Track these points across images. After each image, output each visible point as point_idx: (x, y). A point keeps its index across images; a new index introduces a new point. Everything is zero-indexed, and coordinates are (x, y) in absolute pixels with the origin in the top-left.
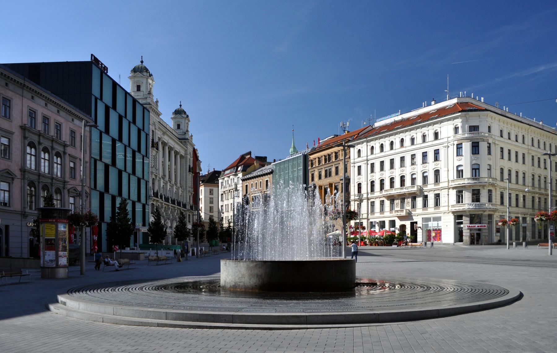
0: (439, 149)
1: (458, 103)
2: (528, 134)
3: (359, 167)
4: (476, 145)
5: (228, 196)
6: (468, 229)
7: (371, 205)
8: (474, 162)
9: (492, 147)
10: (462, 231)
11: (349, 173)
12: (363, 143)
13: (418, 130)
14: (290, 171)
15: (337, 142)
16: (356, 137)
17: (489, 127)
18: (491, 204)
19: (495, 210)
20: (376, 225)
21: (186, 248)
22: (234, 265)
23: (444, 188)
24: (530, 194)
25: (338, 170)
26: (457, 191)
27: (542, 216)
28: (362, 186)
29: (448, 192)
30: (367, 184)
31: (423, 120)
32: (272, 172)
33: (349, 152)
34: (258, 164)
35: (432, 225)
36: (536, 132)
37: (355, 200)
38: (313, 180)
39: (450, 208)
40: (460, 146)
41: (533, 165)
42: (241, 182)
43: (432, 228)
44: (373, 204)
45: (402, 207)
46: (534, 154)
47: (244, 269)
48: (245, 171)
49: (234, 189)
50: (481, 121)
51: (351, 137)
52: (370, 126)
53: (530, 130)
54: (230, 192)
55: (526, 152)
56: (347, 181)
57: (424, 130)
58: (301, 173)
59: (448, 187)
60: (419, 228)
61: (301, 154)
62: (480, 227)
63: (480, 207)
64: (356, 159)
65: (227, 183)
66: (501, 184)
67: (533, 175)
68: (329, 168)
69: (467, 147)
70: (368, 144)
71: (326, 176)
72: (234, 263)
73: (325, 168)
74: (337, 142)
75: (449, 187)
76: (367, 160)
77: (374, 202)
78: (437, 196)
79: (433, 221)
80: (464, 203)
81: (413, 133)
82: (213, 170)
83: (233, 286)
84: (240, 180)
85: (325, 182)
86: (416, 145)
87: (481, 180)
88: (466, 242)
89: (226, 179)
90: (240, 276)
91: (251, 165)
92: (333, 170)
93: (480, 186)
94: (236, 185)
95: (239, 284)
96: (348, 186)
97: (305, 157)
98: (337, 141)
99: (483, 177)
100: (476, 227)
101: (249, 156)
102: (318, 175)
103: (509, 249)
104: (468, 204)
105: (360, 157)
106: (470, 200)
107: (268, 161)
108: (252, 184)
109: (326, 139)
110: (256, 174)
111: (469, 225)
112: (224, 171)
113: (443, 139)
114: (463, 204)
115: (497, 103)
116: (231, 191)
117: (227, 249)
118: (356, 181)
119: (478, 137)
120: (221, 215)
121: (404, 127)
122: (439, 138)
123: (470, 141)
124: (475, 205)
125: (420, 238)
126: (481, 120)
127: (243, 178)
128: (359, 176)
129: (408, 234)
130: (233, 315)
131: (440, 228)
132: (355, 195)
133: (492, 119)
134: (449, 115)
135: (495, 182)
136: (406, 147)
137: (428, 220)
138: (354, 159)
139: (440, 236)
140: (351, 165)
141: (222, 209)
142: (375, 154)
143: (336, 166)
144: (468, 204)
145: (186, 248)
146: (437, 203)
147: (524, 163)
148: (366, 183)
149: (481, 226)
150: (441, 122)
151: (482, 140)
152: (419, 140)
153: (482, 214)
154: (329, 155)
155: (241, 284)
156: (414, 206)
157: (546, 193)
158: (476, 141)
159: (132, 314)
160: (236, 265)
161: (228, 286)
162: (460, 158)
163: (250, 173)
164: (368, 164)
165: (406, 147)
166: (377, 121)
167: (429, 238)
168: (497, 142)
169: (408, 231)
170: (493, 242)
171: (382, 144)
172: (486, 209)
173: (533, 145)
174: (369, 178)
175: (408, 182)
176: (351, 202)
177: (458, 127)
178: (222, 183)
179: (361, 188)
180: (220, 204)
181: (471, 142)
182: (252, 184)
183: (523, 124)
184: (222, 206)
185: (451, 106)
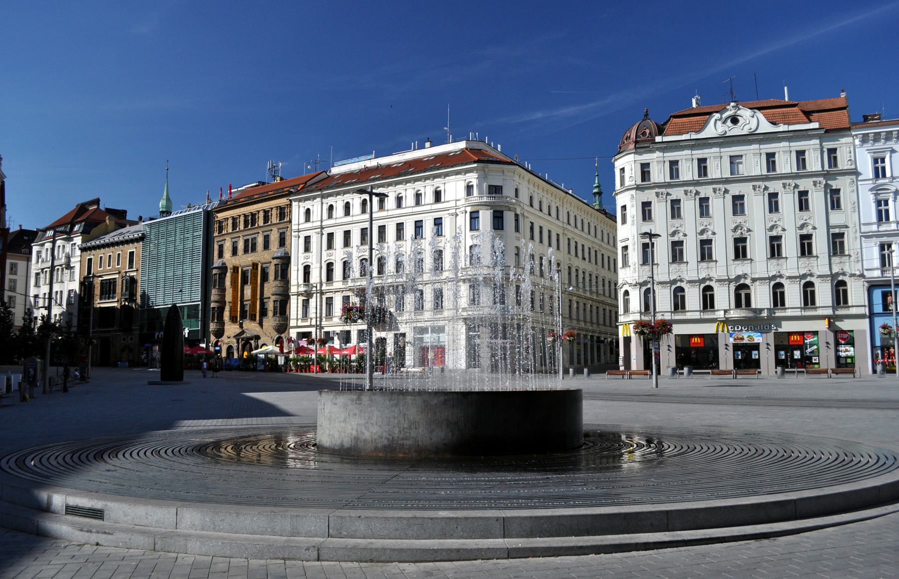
1: (466, 149)
2: (563, 206)
3: (307, 239)
4: (498, 215)
7: (327, 304)
11: (288, 247)
12: (314, 198)
13: (408, 185)
14: (177, 238)
16: (302, 188)
17: (516, 190)
20: (336, 338)
21: (32, 372)
22: (387, 402)
25: (268, 241)
27: (643, 326)
28: (311, 270)
30: (321, 268)
32: (142, 239)
33: (291, 211)
34: (113, 223)
35: (428, 338)
36: (573, 204)
37: (298, 294)
38: (221, 255)
41: (569, 253)
42: (78, 252)
44: (330, 301)
46: (570, 236)
48: (89, 233)
49: (64, 266)
51: (293, 187)
52: (324, 171)
53: (565, 200)
55: (560, 232)
56: (285, 261)
57: (419, 185)
58: (200, 243)
60: (409, 345)
61: (201, 210)
64: (302, 224)
68: (253, 236)
69: (485, 217)
70: (323, 200)
71: (246, 251)
73: (244, 236)
76: (322, 228)
77: (332, 298)
82: (18, 228)
83: (385, 447)
84: (77, 248)
85: (244, 260)
86: (404, 208)
90: (405, 426)
91: (99, 224)
92: (260, 240)
94: (68, 258)
95: (401, 442)
96: (287, 269)
97: (209, 216)
98: (268, 192)
101: (95, 207)
102: (231, 248)
103: (563, 379)
105: (309, 221)
107: (129, 217)
108: (101, 257)
109: (243, 188)
110: (111, 240)
113: (448, 202)
116: (46, 271)
118: (301, 261)
119: (502, 204)
121: (386, 178)
123: (491, 209)
125: (409, 359)
126: (505, 178)
127: (84, 245)
128: (307, 254)
130: (667, 513)
131: (443, 344)
132: (298, 285)
134: (459, 166)
136: (388, 210)
137: (423, 330)
140: (293, 234)
142: (336, 218)
143: (265, 234)
145: (32, 372)
148: (319, 265)
150: (447, 175)
152: (409, 200)
154: (253, 215)
159: (397, 530)
160: (392, 402)
162: (475, 233)
164: (322, 234)
165: (388, 210)
166: (335, 165)
168: (526, 214)
169: (390, 349)
171: (348, 204)
173: (569, 223)
174: (324, 258)
175: (390, 266)
176: (292, 297)
177: (472, 186)
178: (39, 252)
179: (309, 273)
180: (33, 291)
181: (492, 211)
182: (101, 257)
184: (36, 296)
185: (457, 152)
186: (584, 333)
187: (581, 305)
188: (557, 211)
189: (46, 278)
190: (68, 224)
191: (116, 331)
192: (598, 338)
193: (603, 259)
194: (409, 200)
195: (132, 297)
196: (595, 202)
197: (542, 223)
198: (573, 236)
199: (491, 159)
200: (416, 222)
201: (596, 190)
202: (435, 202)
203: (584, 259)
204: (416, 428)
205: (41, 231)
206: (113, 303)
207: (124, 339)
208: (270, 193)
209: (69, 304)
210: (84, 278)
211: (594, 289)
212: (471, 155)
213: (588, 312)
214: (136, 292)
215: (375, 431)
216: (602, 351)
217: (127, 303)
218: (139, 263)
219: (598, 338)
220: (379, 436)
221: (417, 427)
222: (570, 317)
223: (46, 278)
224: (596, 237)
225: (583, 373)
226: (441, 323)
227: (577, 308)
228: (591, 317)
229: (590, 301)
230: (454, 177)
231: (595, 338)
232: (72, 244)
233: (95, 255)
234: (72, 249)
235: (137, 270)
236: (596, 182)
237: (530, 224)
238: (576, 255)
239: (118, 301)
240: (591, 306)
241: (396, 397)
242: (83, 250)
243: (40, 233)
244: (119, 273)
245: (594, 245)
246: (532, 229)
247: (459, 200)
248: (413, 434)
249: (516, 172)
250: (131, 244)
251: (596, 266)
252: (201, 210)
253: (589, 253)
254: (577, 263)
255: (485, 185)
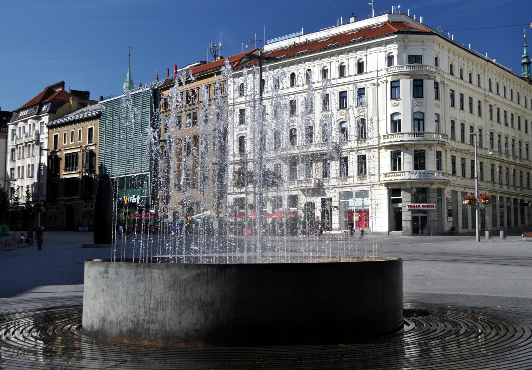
0: (364, 88)
1: (389, 22)
2: (484, 74)
3: (242, 112)
4: (419, 83)
5: (23, 151)
6: (409, 210)
8: (416, 109)
9: (441, 87)
10: (400, 213)
13: (333, 58)
15: (206, 72)
16: (237, 65)
17: (436, 59)
18: (442, 173)
19: (446, 183)
20: (268, 203)
23: (372, 148)
24: (489, 160)
26: (391, 152)
29: (379, 153)
31: (341, 43)
32: (99, 116)
34: (76, 103)
35: (354, 203)
36: (495, 72)
39: (382, 178)
40: (395, 84)
41: (491, 119)
42: (46, 130)
43: (353, 208)
45: (309, 175)
46: (492, 102)
47: (162, 286)
49: (34, 142)
50: (425, 49)
53: (487, 68)
54: (26, 146)
55: (482, 99)
57: (342, 58)
59: (378, 145)
60: (335, 209)
62: (426, 208)
63: (426, 178)
65: (22, 131)
66: (453, 144)
67: (492, 133)
68: (194, 111)
72: (132, 271)
74: (206, 72)
75: (380, 145)
78: (362, 159)
79: (356, 197)
80: (402, 170)
81: (325, 62)
84: (45, 126)
87: (427, 136)
88: (406, 230)
89: (21, 124)
90: (152, 306)
91: (64, 104)
93: (425, 145)
94: (38, 135)
98: (207, 70)
99: (429, 131)
100: (421, 208)
101: (61, 89)
103: (479, 241)
104: (409, 172)
106: (412, 165)
107: (91, 98)
108: (65, 134)
111: (410, 204)
112: (18, 111)
113: (370, 72)
114: (402, 172)
115: (439, 27)
116: (30, 145)
117: (27, 241)
118: (236, 134)
119: (421, 73)
120: (10, 184)
121: (312, 53)
122: (365, 71)
123: (411, 78)
124: (420, 173)
125: (336, 223)
126: (425, 47)
129: (318, 218)
133: (439, 47)
134: (380, 38)
135: (445, 140)
137: (349, 195)
138: (234, 99)
139: (367, 220)
141: (11, 174)
144: (409, 172)
146: (362, 171)
147: (480, 115)
149: (427, 206)
150: (368, 47)
151: (427, 77)
152: (334, 73)
153: (429, 187)
155: (154, 327)
156: (326, 174)
157: (507, 159)
158: (419, 77)
160: (138, 277)
161: (115, 331)
162: (396, 102)
163: (62, 116)
166: (268, 43)
167: (350, 224)
168: (446, 82)
170: (444, 231)
172: (435, 180)
173: (490, 90)
177: (393, 57)
178: (14, 131)
181: (412, 80)
182: (65, 134)
183: (479, 58)
185: (379, 25)
186: (507, 196)
187: (518, 172)
188: (479, 78)
189: (20, 154)
190: (37, 105)
191: (79, 199)
192: (522, 201)
193: (526, 125)
194: (334, 73)
195: (91, 168)
196: (524, 72)
197: (463, 91)
198: (495, 102)
199: (411, 30)
200: (340, 93)
201: (524, 61)
202: (358, 73)
203: (507, 124)
204: (163, 310)
205: (15, 111)
206: (76, 175)
207: (86, 206)
208: (210, 71)
209: (39, 176)
210: (51, 153)
211: (503, 149)
212: (392, 27)
213: (511, 177)
214: (95, 164)
215: (120, 312)
216: (526, 214)
217: (87, 174)
218: (97, 138)
219: (522, 201)
220: (124, 318)
221: (164, 307)
222: (493, 181)
223: (20, 154)
224: (519, 103)
225: (499, 235)
226: (366, 188)
227: (500, 172)
228: (515, 180)
229: (513, 166)
230: (375, 49)
231: (519, 201)
232: (41, 123)
233: (60, 132)
234: (41, 127)
235: (95, 145)
236: (525, 52)
237: (497, 109)
238: (499, 121)
239: (80, 172)
240: (514, 170)
241: (142, 270)
242: (50, 127)
243: (14, 114)
244: (81, 147)
245: (517, 112)
246: (452, 96)
247: (380, 71)
248: (160, 316)
249: (435, 42)
250: (90, 122)
251: (519, 132)
252: (149, 89)
253: (512, 119)
254: (500, 128)
255: (405, 56)
